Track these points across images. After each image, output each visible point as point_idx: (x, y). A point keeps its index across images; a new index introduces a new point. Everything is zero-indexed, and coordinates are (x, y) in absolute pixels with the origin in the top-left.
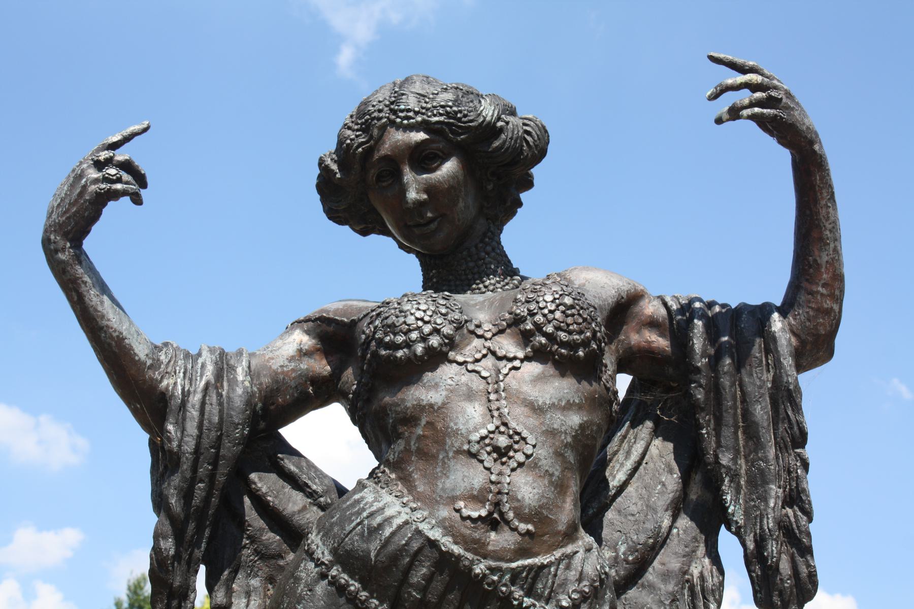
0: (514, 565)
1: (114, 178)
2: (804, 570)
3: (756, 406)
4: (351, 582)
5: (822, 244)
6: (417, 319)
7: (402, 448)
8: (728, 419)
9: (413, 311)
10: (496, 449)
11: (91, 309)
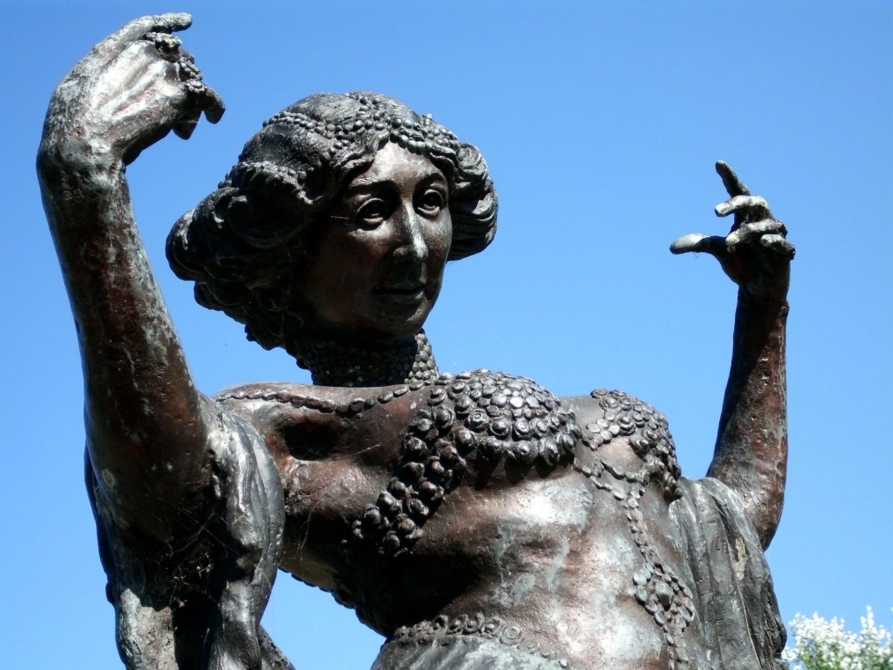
3: (731, 601)
5: (780, 416)
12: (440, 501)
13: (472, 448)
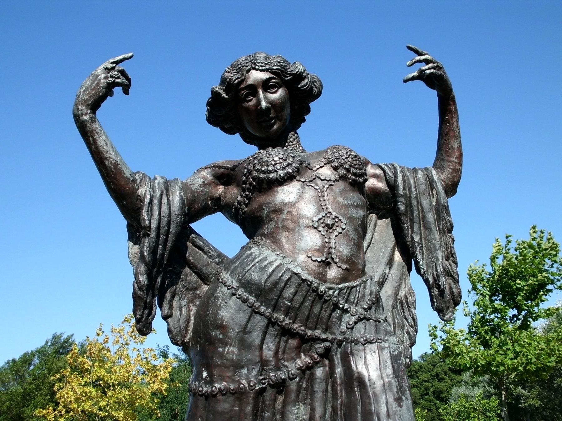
0: (340, 286)
1: (116, 76)
2: (455, 290)
4: (250, 297)
6: (280, 158)
7: (273, 226)
8: (416, 220)
9: (277, 155)
10: (327, 225)
11: (101, 147)
12: (250, 198)
13: (256, 178)
